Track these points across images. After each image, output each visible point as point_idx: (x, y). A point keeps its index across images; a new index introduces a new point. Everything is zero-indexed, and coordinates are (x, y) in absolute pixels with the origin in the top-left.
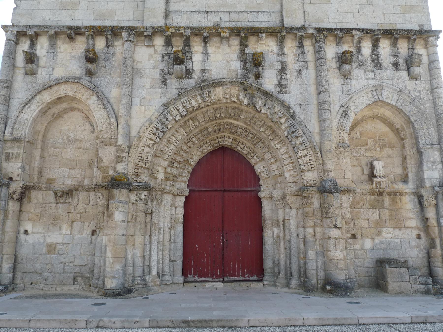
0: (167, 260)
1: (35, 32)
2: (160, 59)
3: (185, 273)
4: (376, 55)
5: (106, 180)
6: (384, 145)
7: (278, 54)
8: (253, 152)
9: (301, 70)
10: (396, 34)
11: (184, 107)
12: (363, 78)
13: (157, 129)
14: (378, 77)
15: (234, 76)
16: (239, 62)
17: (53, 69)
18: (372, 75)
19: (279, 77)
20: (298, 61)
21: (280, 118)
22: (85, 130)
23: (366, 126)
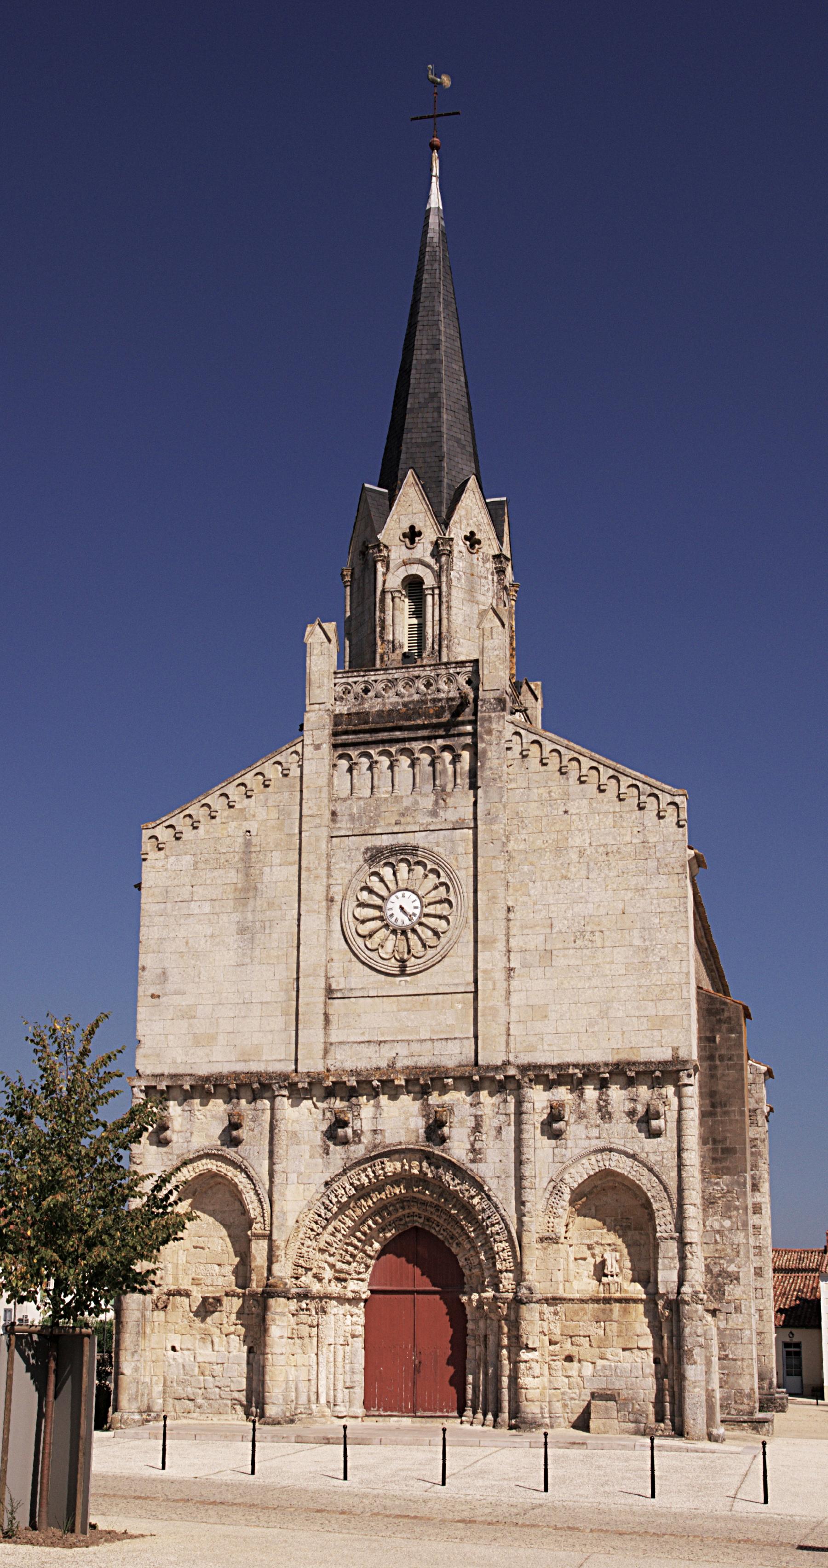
0: (340, 1386)
1: (167, 1087)
2: (321, 1117)
3: (367, 1405)
4: (604, 1101)
5: (261, 1284)
6: (629, 1227)
7: (471, 1105)
8: (452, 1238)
9: (501, 1128)
10: (630, 1070)
11: (352, 1184)
12: (584, 1137)
13: (320, 1216)
14: (604, 1135)
15: (413, 1140)
16: (421, 1118)
17: (192, 1133)
18: (595, 1132)
19: (472, 1138)
20: (497, 1113)
21: (473, 1197)
22: (234, 1210)
23: (605, 1198)
